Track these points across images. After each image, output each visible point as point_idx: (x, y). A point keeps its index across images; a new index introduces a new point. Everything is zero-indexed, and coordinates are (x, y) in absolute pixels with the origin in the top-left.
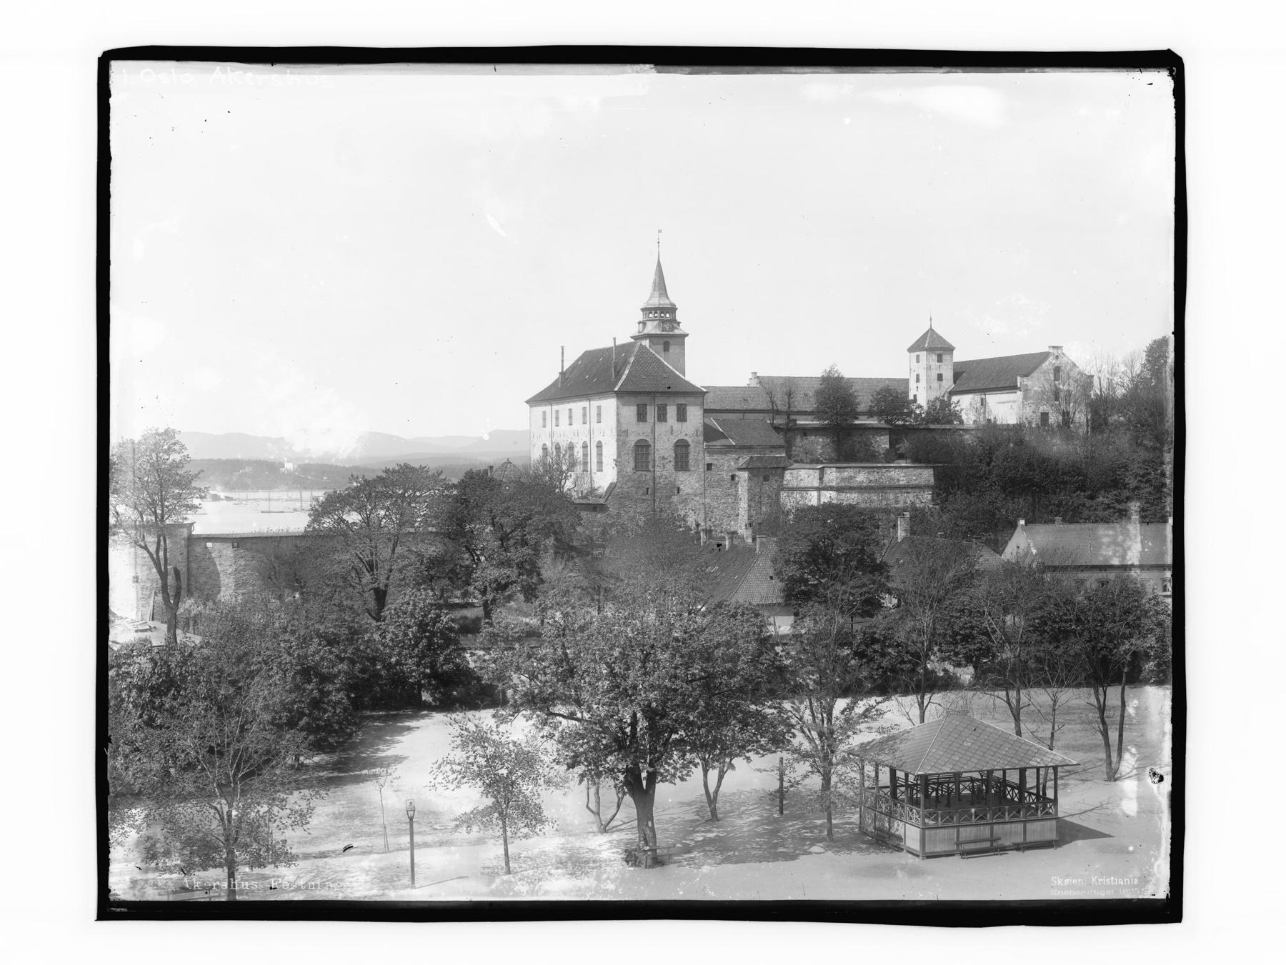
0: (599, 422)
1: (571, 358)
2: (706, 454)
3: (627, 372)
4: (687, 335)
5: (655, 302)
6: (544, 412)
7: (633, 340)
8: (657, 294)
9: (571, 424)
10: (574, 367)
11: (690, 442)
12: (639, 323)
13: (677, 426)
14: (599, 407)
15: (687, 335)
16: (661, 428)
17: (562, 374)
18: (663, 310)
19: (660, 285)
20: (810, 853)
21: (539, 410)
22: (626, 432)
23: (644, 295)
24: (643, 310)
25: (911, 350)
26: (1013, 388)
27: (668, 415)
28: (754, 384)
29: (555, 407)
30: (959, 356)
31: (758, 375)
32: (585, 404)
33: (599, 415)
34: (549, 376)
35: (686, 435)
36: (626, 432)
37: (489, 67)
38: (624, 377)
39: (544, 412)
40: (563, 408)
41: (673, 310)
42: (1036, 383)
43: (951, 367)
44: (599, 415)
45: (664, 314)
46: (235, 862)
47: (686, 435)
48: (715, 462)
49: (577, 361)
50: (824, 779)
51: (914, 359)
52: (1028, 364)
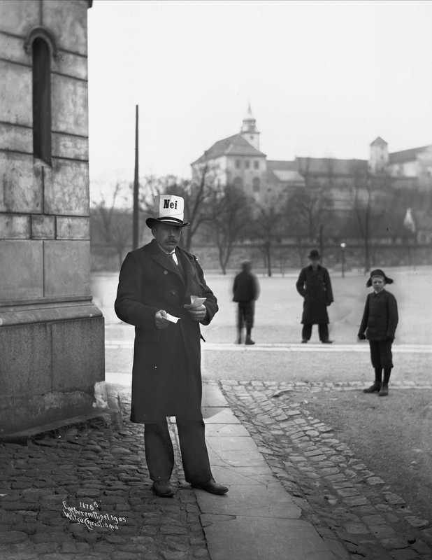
16: (247, 171)
19: (250, 110)
34: (113, 196)
45: (251, 123)
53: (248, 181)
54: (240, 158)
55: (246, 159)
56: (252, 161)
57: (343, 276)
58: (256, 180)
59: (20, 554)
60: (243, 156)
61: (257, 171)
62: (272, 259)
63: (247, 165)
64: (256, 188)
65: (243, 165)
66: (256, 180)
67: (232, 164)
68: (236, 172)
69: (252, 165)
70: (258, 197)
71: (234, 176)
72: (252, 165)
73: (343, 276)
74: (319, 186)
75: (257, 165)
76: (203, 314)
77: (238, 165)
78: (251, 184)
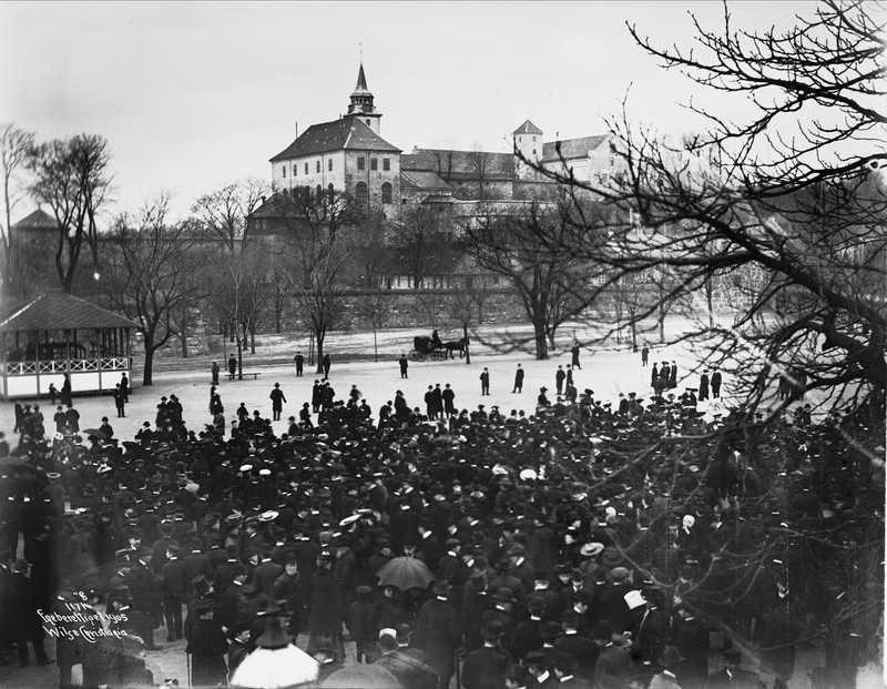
0: (331, 170)
5: (361, 91)
6: (284, 168)
9: (307, 173)
13: (383, 173)
14: (330, 161)
16: (374, 174)
19: (362, 81)
21: (280, 165)
22: (351, 176)
23: (351, 87)
24: (352, 97)
29: (294, 162)
32: (319, 158)
33: (331, 166)
34: (286, 140)
36: (351, 176)
37: (87, 399)
39: (284, 168)
40: (300, 163)
41: (371, 98)
44: (331, 166)
45: (366, 101)
46: (276, 195)
50: (452, 404)
53: (375, 189)
54: (363, 154)
55: (372, 156)
56: (380, 158)
57: (468, 362)
58: (387, 186)
59: (379, 417)
60: (369, 151)
61: (388, 173)
62: (483, 309)
63: (374, 165)
64: (387, 199)
65: (367, 166)
66: (387, 186)
67: (353, 163)
68: (359, 176)
69: (380, 165)
70: (390, 211)
71: (355, 181)
72: (380, 165)
73: (468, 362)
74: (726, 655)
75: (387, 166)
76: (163, 370)
77: (361, 165)
78: (379, 192)
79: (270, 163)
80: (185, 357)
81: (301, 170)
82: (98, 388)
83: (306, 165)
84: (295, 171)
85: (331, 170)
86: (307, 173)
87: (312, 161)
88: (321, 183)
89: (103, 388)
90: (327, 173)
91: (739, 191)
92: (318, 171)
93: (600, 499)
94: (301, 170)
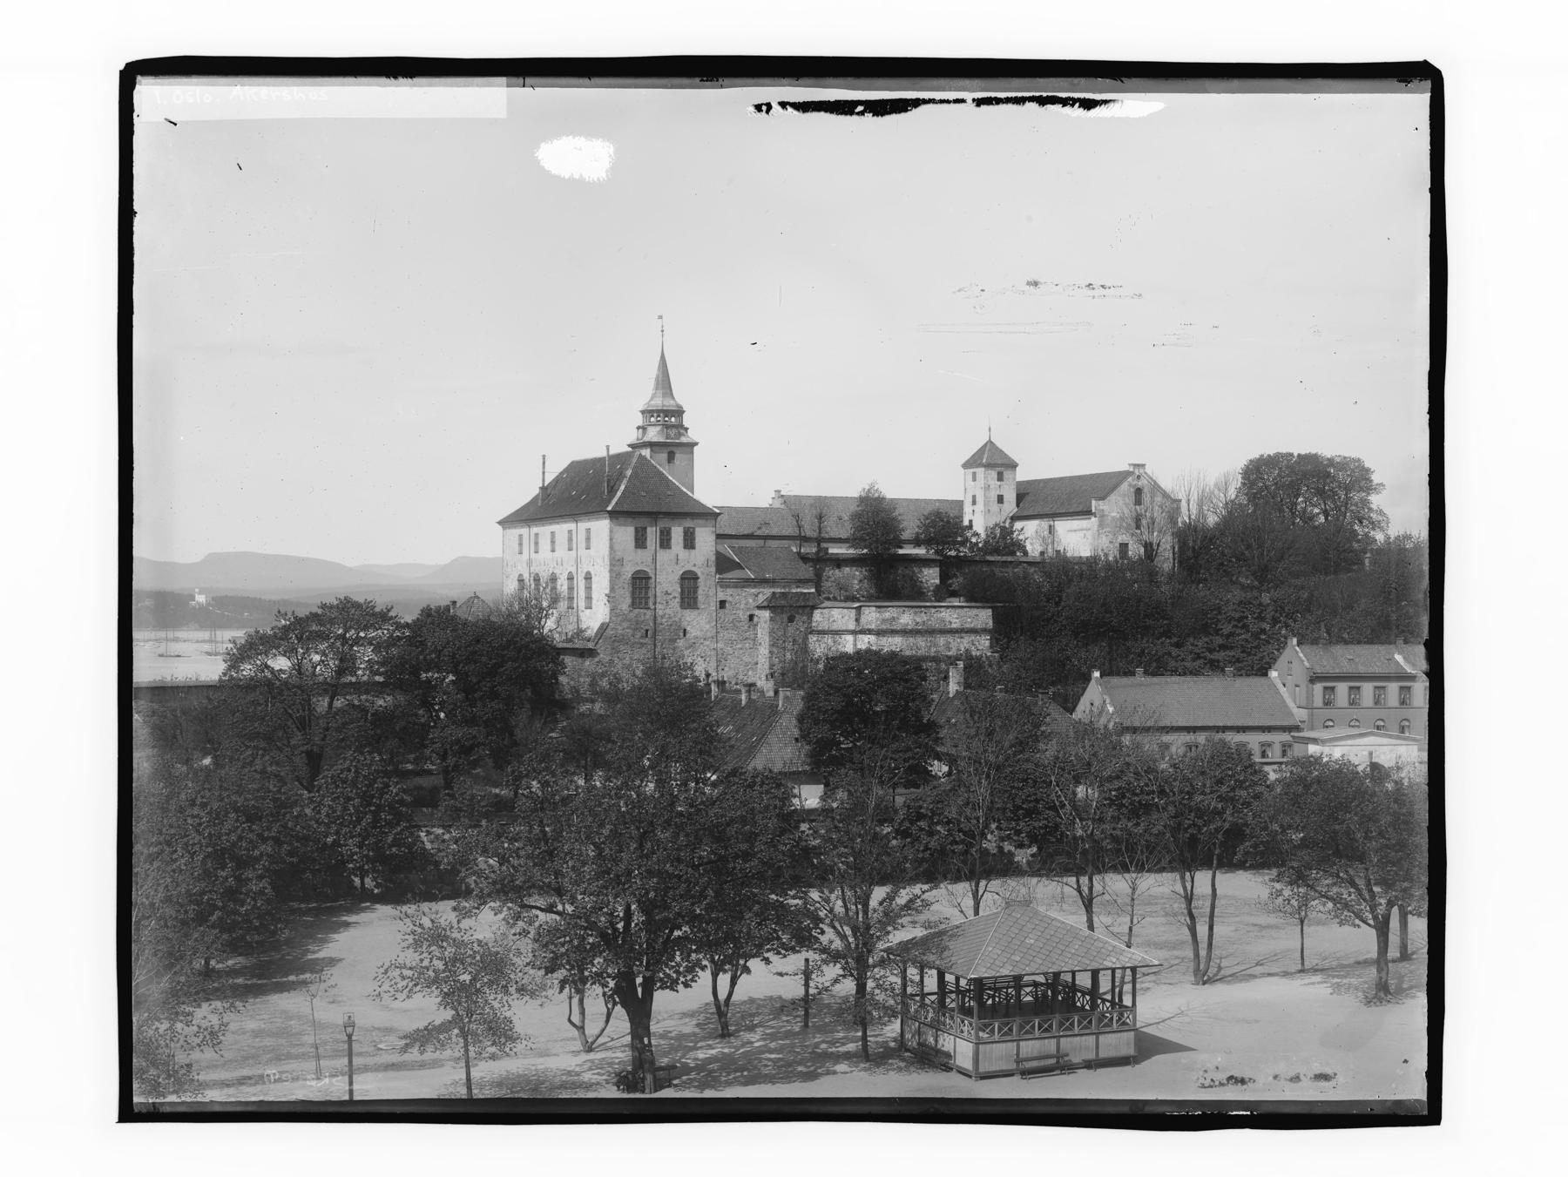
0: (588, 548)
1: (555, 469)
2: (719, 588)
3: (623, 487)
4: (696, 444)
5: (658, 403)
7: (630, 449)
8: (660, 392)
10: (557, 480)
11: (699, 574)
12: (638, 428)
14: (588, 530)
15: (696, 444)
16: (664, 555)
17: (543, 489)
18: (667, 413)
19: (664, 382)
20: (835, 1073)
21: (514, 532)
23: (644, 394)
24: (643, 412)
25: (966, 465)
26: (1087, 513)
27: (673, 541)
28: (778, 504)
29: (535, 530)
30: (1022, 475)
31: (782, 493)
32: (571, 526)
33: (588, 539)
34: (526, 491)
35: (695, 565)
36: (621, 561)
38: (619, 494)
40: (544, 531)
41: (679, 412)
42: (1116, 506)
43: (1013, 487)
44: (588, 539)
45: (668, 416)
47: (695, 565)
48: (729, 599)
49: (562, 473)
51: (970, 477)
52: (1103, 485)
75: (689, 542)
78: (676, 589)
79: (500, 527)
80: (1204, 976)
81: (545, 544)
82: (346, 1098)
83: (553, 534)
84: (536, 543)
85: (588, 548)
86: (553, 551)
87: (562, 529)
88: (573, 570)
89: (357, 1097)
90: (582, 552)
91: (1396, 782)
92: (570, 549)
93: (197, 754)
94: (545, 544)
